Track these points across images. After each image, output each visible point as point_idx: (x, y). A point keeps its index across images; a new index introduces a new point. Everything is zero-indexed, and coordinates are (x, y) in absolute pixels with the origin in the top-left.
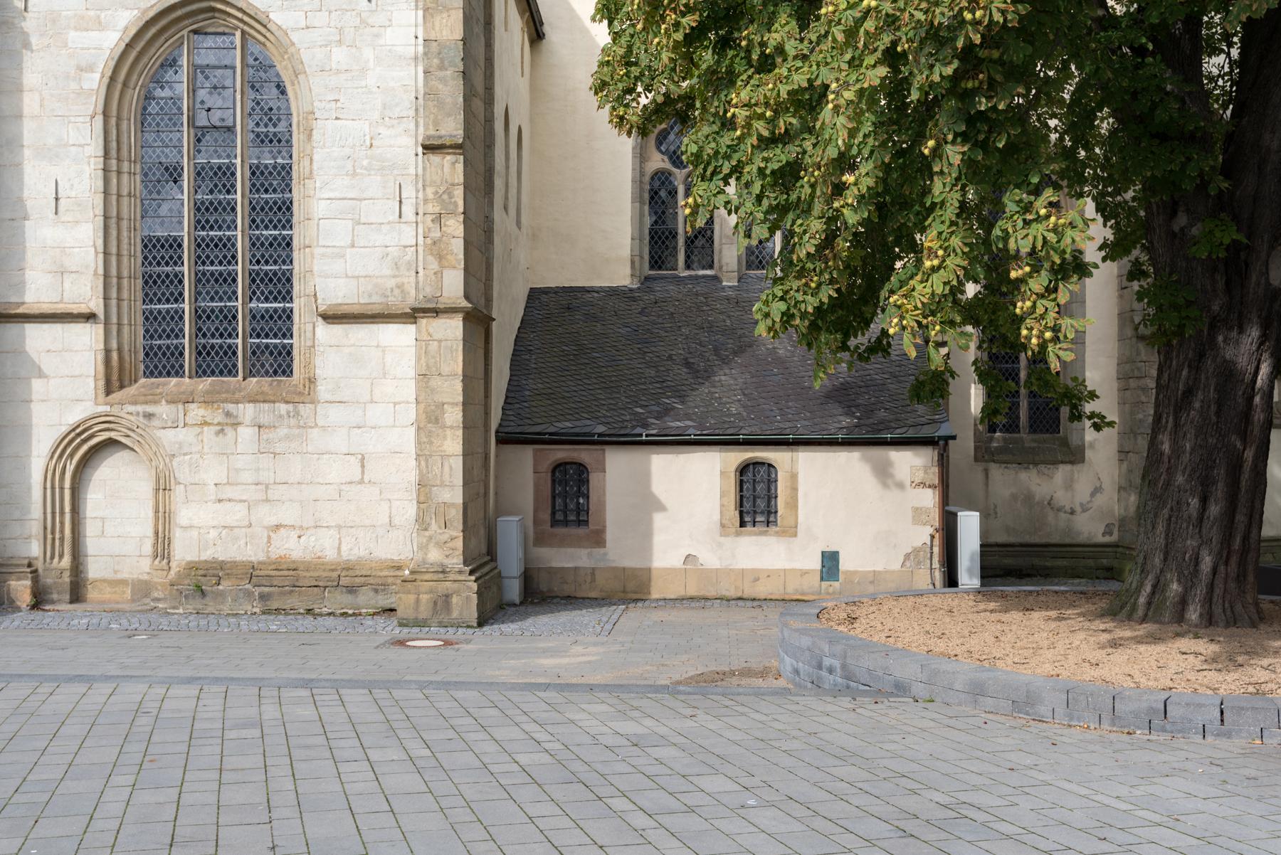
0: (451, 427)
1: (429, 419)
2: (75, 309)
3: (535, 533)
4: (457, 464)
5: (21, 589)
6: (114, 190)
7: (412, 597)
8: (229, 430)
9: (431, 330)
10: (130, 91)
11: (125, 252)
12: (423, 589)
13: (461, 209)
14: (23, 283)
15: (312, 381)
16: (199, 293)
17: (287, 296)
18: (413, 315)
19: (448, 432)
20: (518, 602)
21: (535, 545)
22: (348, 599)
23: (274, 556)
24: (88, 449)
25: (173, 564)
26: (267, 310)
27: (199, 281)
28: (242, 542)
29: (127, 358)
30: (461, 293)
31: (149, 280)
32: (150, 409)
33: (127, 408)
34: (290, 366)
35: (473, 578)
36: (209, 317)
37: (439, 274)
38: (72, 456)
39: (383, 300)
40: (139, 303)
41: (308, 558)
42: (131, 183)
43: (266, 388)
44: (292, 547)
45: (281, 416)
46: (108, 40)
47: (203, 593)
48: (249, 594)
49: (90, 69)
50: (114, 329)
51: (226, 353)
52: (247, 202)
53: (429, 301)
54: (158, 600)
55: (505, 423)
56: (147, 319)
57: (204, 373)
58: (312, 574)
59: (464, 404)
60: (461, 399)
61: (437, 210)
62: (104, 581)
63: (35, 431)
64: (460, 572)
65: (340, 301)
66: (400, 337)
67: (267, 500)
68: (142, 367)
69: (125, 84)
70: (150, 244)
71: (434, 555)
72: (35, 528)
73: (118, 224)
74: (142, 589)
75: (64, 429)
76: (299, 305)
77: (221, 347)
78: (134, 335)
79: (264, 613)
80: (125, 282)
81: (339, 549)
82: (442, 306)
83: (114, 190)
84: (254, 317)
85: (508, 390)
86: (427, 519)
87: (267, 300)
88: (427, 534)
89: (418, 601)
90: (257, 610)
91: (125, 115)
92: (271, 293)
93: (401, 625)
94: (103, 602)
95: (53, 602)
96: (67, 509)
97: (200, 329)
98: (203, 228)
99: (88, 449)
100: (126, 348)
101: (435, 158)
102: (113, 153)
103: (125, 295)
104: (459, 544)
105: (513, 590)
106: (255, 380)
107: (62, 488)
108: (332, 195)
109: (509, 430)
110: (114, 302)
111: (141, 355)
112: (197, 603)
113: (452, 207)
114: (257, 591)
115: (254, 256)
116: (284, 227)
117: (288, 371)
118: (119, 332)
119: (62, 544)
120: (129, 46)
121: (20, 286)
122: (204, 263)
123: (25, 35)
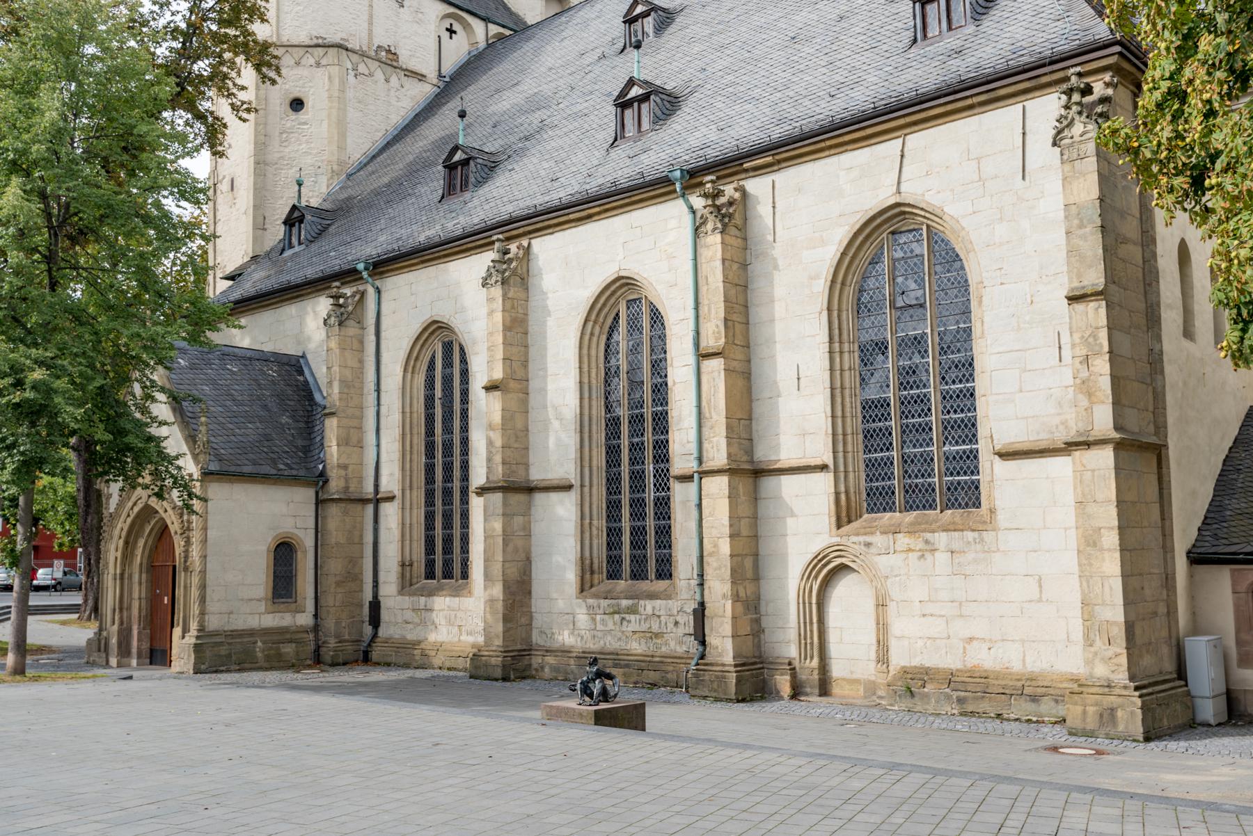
0: (1109, 550)
1: (1090, 541)
2: (813, 462)
3: (1239, 653)
4: (1117, 584)
5: (783, 683)
6: (838, 367)
7: (1079, 709)
8: (928, 555)
9: (1084, 462)
10: (847, 288)
11: (848, 414)
12: (1088, 702)
13: (1106, 349)
14: (779, 444)
15: (992, 511)
16: (904, 442)
17: (973, 438)
18: (1070, 446)
19: (1107, 555)
20: (1212, 722)
21: (1239, 666)
22: (1031, 707)
23: (969, 666)
24: (828, 572)
25: (891, 668)
26: (957, 452)
27: (904, 432)
28: (943, 651)
29: (853, 498)
30: (1111, 425)
31: (868, 435)
32: (868, 539)
33: (852, 539)
34: (978, 499)
35: (1137, 693)
36: (912, 461)
37: (1089, 410)
38: (816, 577)
39: (1050, 436)
40: (861, 453)
41: (998, 668)
42: (852, 359)
43: (958, 519)
44: (984, 659)
45: (969, 542)
46: (829, 253)
47: (912, 694)
48: (948, 697)
49: (817, 277)
50: (842, 475)
51: (927, 490)
52: (937, 363)
53: (1081, 435)
54: (881, 697)
55: (1198, 544)
56: (867, 466)
57: (911, 507)
58: (1000, 682)
59: (1120, 528)
60: (1116, 523)
61: (1084, 352)
62: (844, 679)
63: (790, 558)
64: (1125, 687)
65: (1012, 440)
66: (1061, 466)
67: (961, 616)
68: (865, 505)
69: (843, 284)
70: (867, 406)
71: (1101, 671)
72: (792, 634)
73: (842, 393)
74: (871, 688)
75: (810, 557)
76: (983, 447)
77: (923, 485)
78: (858, 480)
79: (961, 714)
80: (849, 437)
81: (1024, 661)
82: (1091, 439)
83: (838, 367)
84: (947, 459)
85: (1208, 511)
86: (1092, 636)
87: (957, 443)
88: (1092, 649)
89: (1084, 712)
90: (955, 711)
91: (844, 307)
92: (960, 437)
93: (1071, 734)
94: (844, 697)
95: (807, 694)
96: (815, 620)
97: (906, 472)
98: (905, 389)
99: (828, 572)
100: (852, 490)
101: (1079, 307)
102: (836, 338)
103: (850, 448)
104: (1124, 660)
105: (1209, 710)
106: (950, 512)
107: (810, 603)
108: (1001, 349)
109: (1202, 550)
110: (841, 455)
111: (864, 496)
112: (906, 703)
113: (1097, 348)
114: (955, 694)
115: (945, 407)
116: (968, 381)
117: (977, 505)
118: (846, 477)
119: (812, 649)
120: (844, 254)
121: (777, 447)
122: (907, 417)
123: (775, 259)
